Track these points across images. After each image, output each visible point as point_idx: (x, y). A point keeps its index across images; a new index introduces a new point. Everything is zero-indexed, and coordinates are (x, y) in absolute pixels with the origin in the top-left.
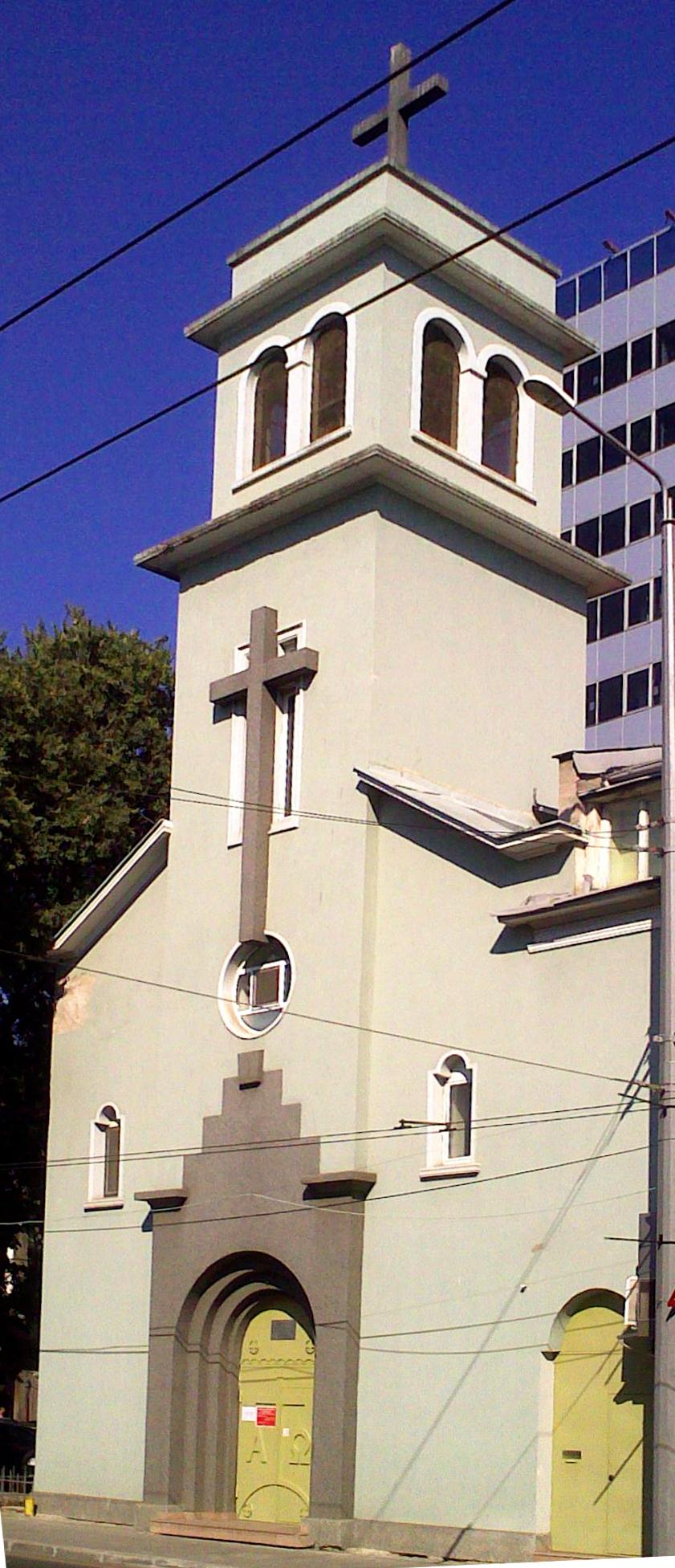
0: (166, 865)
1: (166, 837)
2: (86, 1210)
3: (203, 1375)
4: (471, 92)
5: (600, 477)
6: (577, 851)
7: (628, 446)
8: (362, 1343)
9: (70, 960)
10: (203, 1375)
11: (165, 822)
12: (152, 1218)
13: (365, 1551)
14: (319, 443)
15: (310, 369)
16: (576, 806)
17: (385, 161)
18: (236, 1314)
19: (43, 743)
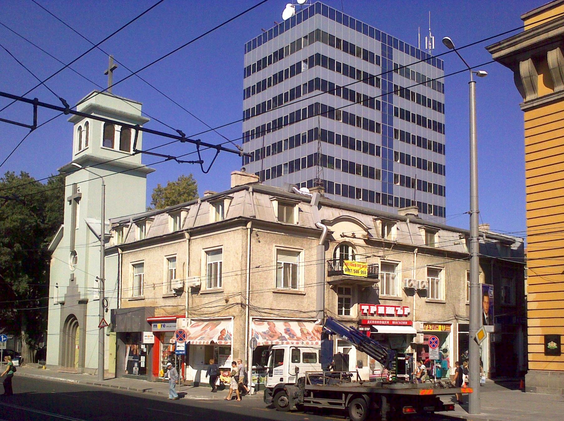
0: (63, 236)
1: (63, 228)
2: (54, 304)
3: (69, 339)
4: (187, 320)
5: (295, 76)
6: (111, 238)
7: (419, 48)
8: (87, 332)
9: (51, 252)
10: (69, 339)
11: (62, 225)
12: (140, 153)
13: (85, 374)
14: (398, 262)
15: (86, 132)
16: (111, 230)
17: (95, 90)
18: (74, 326)
19: (22, 207)
